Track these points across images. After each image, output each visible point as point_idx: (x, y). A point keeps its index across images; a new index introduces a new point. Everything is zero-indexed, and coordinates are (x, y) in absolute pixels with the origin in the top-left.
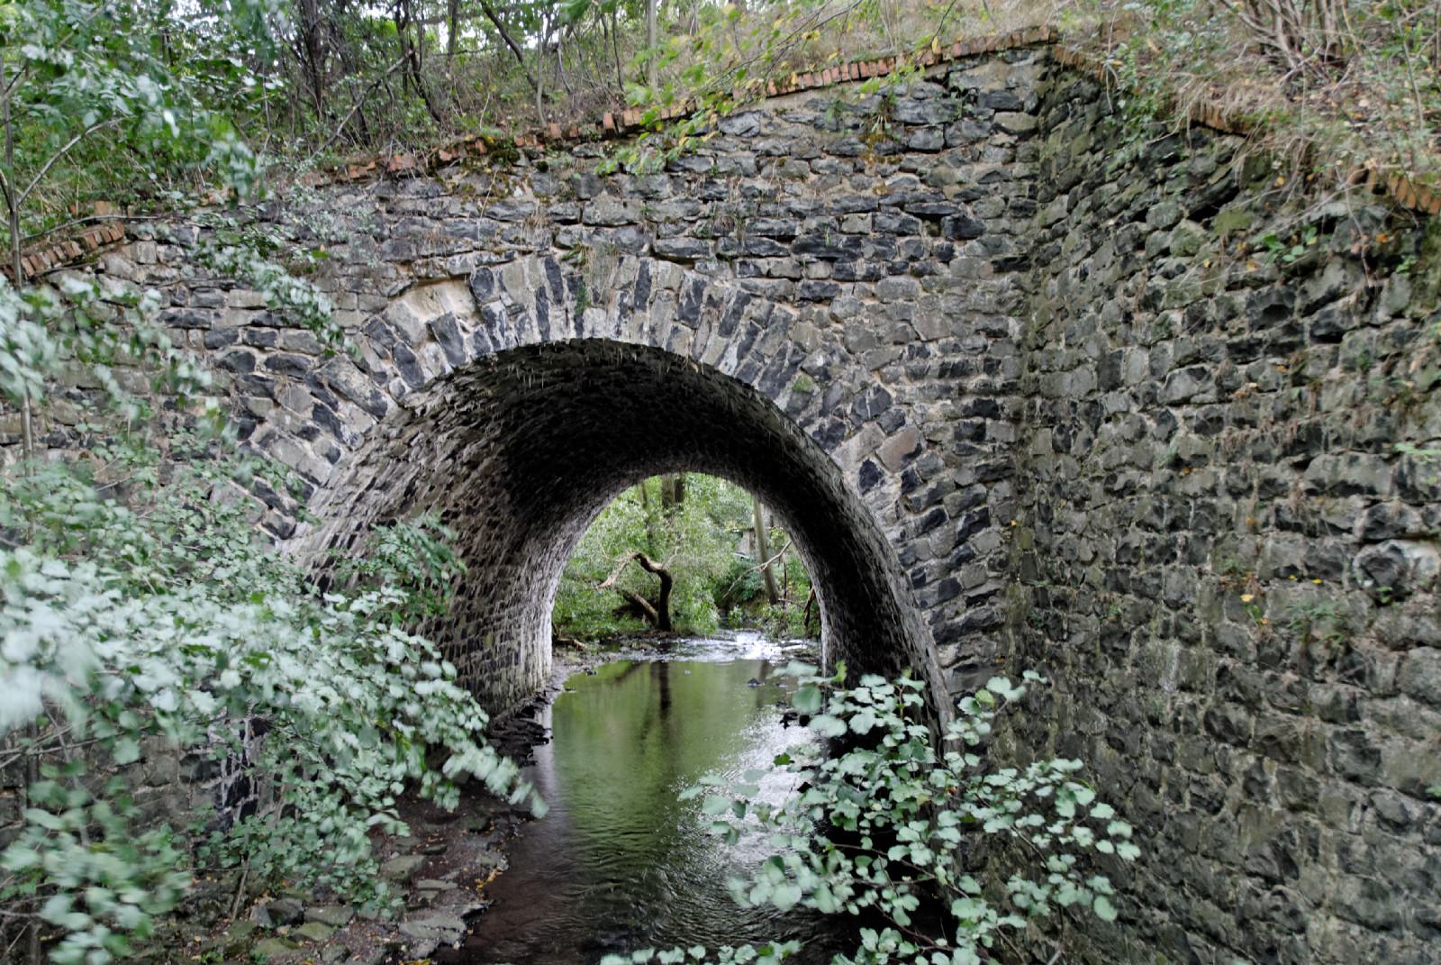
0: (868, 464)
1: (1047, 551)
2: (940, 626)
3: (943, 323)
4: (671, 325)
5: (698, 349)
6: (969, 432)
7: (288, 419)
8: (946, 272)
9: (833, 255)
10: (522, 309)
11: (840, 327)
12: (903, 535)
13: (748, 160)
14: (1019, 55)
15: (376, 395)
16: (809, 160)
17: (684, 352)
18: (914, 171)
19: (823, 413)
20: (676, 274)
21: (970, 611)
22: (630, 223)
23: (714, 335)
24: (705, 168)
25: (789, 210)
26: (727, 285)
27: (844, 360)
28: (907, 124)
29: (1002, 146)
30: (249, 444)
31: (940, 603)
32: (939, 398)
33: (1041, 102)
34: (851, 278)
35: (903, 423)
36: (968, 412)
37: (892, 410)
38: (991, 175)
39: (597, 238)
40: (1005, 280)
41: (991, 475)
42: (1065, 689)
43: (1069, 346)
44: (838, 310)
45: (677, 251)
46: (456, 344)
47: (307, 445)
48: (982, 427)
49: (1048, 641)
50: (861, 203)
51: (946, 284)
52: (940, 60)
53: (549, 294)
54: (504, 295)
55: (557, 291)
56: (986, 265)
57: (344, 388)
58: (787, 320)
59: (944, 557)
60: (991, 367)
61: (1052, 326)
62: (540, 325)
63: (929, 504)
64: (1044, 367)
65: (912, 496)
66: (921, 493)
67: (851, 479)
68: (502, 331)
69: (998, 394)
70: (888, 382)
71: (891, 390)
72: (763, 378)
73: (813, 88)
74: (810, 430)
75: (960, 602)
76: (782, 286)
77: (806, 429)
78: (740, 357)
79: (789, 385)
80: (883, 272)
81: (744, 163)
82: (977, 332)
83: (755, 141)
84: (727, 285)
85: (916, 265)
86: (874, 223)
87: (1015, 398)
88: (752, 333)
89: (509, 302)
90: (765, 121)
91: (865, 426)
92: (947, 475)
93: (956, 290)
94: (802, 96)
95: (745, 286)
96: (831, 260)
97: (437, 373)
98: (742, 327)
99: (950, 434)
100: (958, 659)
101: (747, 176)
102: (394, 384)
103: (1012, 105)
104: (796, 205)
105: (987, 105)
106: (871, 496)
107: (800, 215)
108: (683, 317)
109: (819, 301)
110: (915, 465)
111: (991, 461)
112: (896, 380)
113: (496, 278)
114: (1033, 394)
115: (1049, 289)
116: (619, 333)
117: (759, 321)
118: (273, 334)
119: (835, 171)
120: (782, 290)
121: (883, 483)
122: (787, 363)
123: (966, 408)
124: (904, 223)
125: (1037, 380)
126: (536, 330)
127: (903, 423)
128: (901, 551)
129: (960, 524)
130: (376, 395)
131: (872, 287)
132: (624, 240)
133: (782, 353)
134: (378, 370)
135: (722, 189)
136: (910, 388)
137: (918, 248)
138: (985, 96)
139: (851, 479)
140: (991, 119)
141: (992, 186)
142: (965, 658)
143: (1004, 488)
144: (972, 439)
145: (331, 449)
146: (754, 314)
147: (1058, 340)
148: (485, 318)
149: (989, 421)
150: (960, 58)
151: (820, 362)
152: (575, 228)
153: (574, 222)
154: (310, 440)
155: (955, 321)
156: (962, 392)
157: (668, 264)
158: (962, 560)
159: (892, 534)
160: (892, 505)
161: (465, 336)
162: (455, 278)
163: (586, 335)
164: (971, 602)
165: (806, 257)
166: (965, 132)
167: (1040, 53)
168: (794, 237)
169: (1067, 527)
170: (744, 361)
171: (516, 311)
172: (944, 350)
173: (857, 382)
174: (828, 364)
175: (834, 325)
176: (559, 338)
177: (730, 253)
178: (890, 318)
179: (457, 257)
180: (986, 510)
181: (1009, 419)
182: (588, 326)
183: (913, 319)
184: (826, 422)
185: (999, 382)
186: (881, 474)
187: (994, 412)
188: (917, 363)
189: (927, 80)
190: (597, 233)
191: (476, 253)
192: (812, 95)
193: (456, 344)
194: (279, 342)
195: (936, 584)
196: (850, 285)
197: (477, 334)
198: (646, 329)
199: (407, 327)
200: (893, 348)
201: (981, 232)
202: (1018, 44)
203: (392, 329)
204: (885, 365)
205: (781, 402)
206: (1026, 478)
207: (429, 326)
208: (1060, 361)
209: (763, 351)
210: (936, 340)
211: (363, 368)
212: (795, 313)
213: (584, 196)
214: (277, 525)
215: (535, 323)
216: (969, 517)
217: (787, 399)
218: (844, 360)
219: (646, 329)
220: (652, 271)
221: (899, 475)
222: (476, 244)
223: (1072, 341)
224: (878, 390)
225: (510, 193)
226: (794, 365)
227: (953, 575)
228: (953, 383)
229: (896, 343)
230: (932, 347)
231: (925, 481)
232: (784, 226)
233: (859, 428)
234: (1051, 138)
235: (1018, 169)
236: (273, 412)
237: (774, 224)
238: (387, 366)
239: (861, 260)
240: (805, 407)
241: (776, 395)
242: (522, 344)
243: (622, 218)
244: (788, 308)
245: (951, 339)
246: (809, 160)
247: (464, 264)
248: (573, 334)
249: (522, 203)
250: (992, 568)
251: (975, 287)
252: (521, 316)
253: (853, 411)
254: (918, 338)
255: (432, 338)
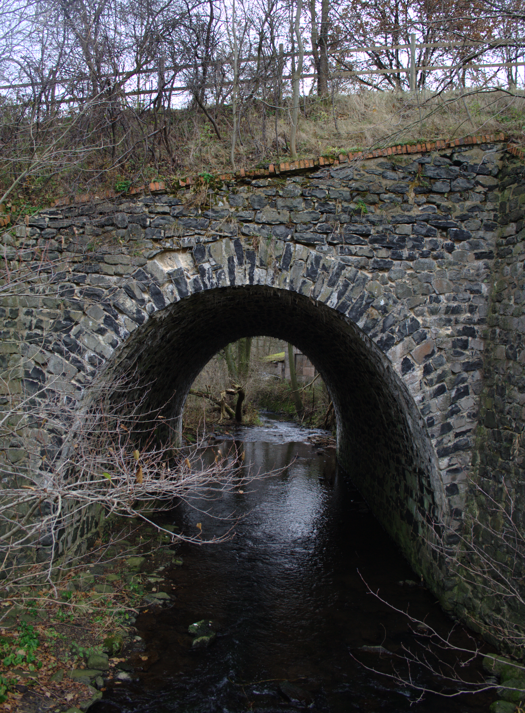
0: (406, 360)
1: (502, 412)
2: (441, 447)
3: (448, 284)
4: (301, 280)
5: (316, 293)
6: (460, 344)
7: (91, 323)
8: (450, 257)
9: (391, 245)
10: (220, 268)
11: (393, 284)
12: (423, 399)
13: (346, 192)
14: (489, 146)
15: (139, 312)
16: (379, 194)
17: (309, 294)
18: (434, 203)
19: (383, 331)
20: (305, 252)
21: (457, 439)
22: (281, 223)
23: (325, 285)
24: (323, 195)
25: (368, 220)
26: (333, 259)
27: (395, 302)
28: (431, 178)
29: (480, 193)
30: (69, 336)
31: (441, 435)
32: (445, 325)
33: (500, 171)
34: (400, 258)
35: (425, 338)
36: (459, 333)
37: (420, 330)
38: (473, 209)
39: (264, 231)
40: (480, 263)
41: (469, 367)
42: (510, 486)
43: (516, 303)
44: (393, 276)
45: (307, 239)
46: (184, 285)
47: (100, 337)
48: (467, 341)
49: (500, 459)
50: (406, 218)
51: (450, 264)
52: (449, 146)
53: (235, 260)
54: (211, 259)
55: (240, 259)
56: (471, 255)
57: (121, 307)
58: (365, 279)
59: (444, 410)
60: (472, 309)
61: (506, 291)
62: (230, 277)
63: (437, 383)
64: (502, 312)
65: (428, 377)
66: (433, 376)
67: (397, 366)
68: (209, 279)
69: (475, 324)
70: (418, 316)
71: (420, 320)
72: (351, 311)
73: (381, 156)
74: (376, 340)
75: (451, 434)
76: (363, 261)
77: (373, 339)
78: (339, 298)
79: (365, 315)
80: (417, 255)
81: (344, 193)
82: (466, 290)
83: (350, 183)
84: (333, 259)
85: (435, 253)
86: (413, 229)
87: (485, 327)
88: (346, 286)
89: (213, 263)
90: (356, 172)
91: (405, 339)
92: (447, 367)
93: (456, 267)
94: (376, 160)
95: (343, 260)
96: (389, 248)
97: (172, 301)
98: (341, 282)
99: (450, 345)
100: (449, 465)
101: (346, 201)
102: (149, 305)
103: (485, 172)
104: (372, 218)
105: (473, 171)
106: (407, 377)
107: (373, 223)
108: (308, 275)
109: (382, 269)
110: (431, 361)
111: (471, 360)
112: (422, 314)
113: (207, 250)
114: (495, 326)
115: (505, 271)
116: (273, 283)
117: (349, 279)
118: (85, 277)
119: (392, 201)
120: (362, 263)
121: (413, 370)
122: (364, 303)
123: (459, 331)
124: (429, 230)
125: (497, 319)
126: (228, 279)
127: (425, 338)
128: (422, 407)
129: (453, 393)
130: (139, 312)
131: (411, 264)
132: (278, 232)
133: (362, 297)
134: (140, 298)
135: (332, 207)
136: (430, 319)
137: (436, 244)
138: (471, 166)
139: (397, 366)
140: (474, 178)
141: (475, 213)
142: (453, 465)
143: (477, 375)
144: (461, 348)
145: (113, 340)
146: (347, 275)
147: (510, 299)
148: (201, 272)
149: (470, 339)
150: (460, 146)
151: (382, 303)
152: (252, 225)
153: (250, 221)
154: (102, 334)
155: (454, 283)
156: (457, 322)
157: (302, 246)
158: (453, 413)
159: (417, 398)
160: (418, 382)
161: (188, 281)
162: (184, 250)
163: (255, 283)
164: (457, 435)
165: (377, 246)
166: (461, 184)
167: (500, 146)
168: (370, 235)
169: (514, 400)
170: (341, 301)
171: (216, 269)
172: (448, 299)
173: (402, 314)
174: (386, 304)
175: (390, 283)
176: (240, 284)
177: (335, 242)
178: (420, 281)
179: (186, 238)
180: (467, 387)
181: (481, 338)
182: (256, 278)
183: (433, 282)
184: (384, 336)
185: (476, 317)
186: (413, 365)
187: (472, 333)
188: (434, 305)
189: (441, 156)
190: (262, 228)
191: (196, 236)
192: (382, 160)
193: (184, 285)
194: (88, 281)
195: (439, 425)
196: (399, 262)
197: (195, 280)
198: (288, 281)
199: (157, 275)
200: (421, 297)
201: (469, 237)
202: (489, 141)
203: (149, 276)
204: (417, 306)
205: (361, 324)
206: (489, 370)
207: (169, 274)
208: (510, 311)
209: (351, 296)
210: (444, 294)
211: (132, 296)
212: (370, 276)
213: (256, 207)
214: (83, 380)
215: (227, 275)
216: (458, 390)
217: (364, 322)
218: (395, 302)
219: (288, 281)
220: (292, 249)
221: (422, 366)
222: (197, 231)
223: (519, 301)
224: (413, 319)
225: (217, 204)
226: (368, 304)
227: (449, 420)
228: (453, 317)
229: (423, 295)
230: (442, 297)
231: (436, 370)
232: (365, 229)
233: (402, 340)
234: (506, 192)
235: (489, 206)
236: (82, 319)
237: (359, 227)
238: (146, 297)
239: (406, 249)
240: (373, 327)
241: (358, 320)
242: (220, 286)
243: (277, 220)
244: (365, 273)
245: (452, 294)
246: (379, 194)
247: (189, 241)
248: (248, 282)
249: (223, 210)
250: (469, 417)
251: (465, 266)
252: (219, 271)
253: (399, 330)
254: (434, 292)
255: (171, 282)
